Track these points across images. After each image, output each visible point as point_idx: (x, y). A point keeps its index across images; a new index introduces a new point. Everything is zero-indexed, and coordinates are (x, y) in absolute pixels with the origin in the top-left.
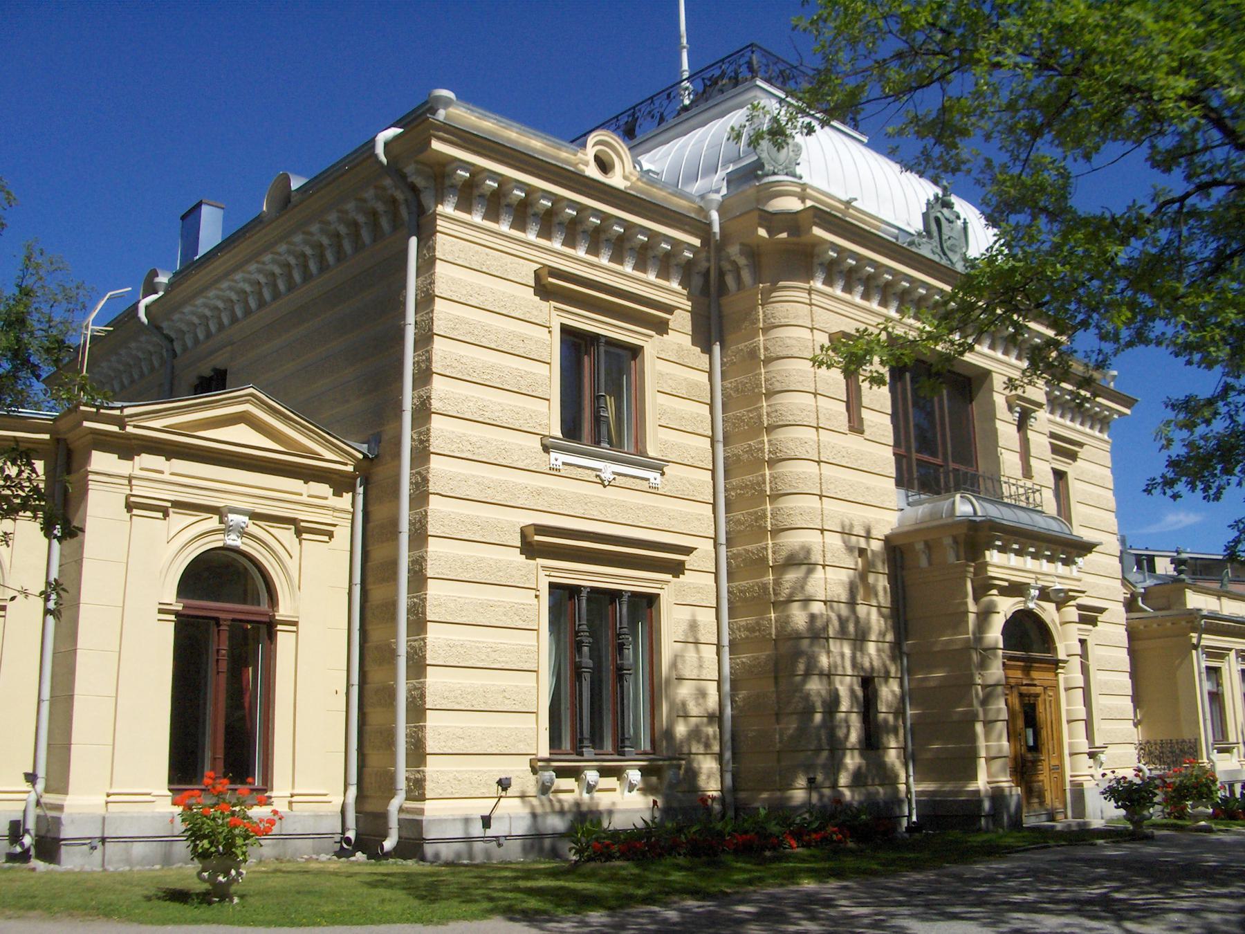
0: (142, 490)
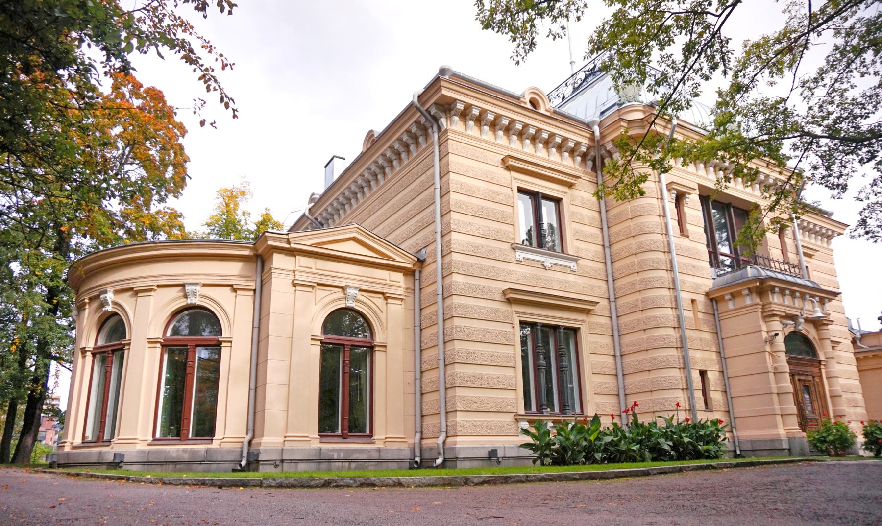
0: (301, 277)
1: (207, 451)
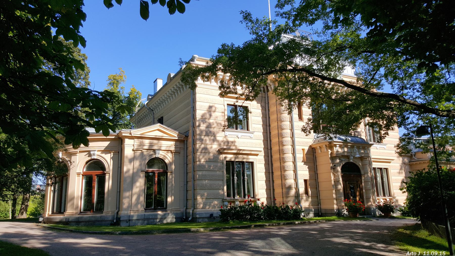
1: (101, 217)
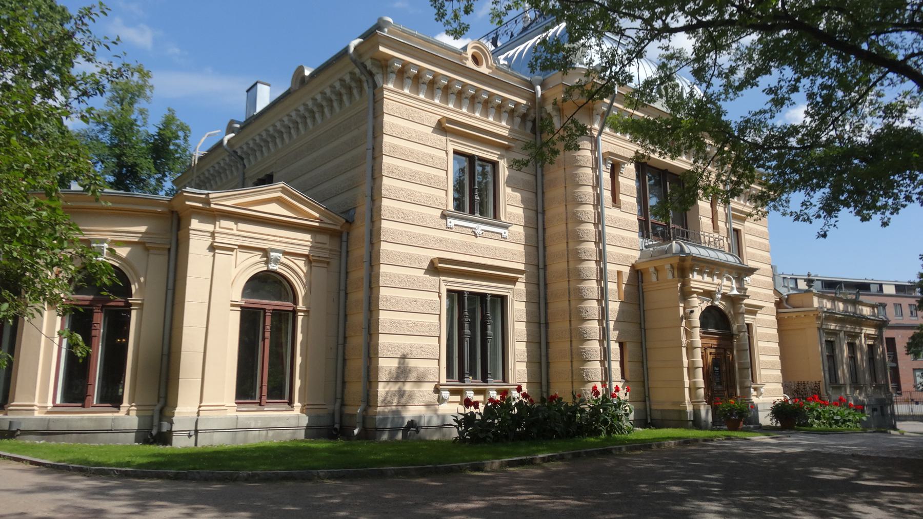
1: (113, 420)
